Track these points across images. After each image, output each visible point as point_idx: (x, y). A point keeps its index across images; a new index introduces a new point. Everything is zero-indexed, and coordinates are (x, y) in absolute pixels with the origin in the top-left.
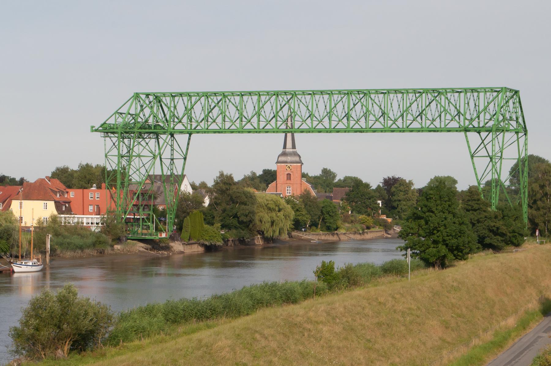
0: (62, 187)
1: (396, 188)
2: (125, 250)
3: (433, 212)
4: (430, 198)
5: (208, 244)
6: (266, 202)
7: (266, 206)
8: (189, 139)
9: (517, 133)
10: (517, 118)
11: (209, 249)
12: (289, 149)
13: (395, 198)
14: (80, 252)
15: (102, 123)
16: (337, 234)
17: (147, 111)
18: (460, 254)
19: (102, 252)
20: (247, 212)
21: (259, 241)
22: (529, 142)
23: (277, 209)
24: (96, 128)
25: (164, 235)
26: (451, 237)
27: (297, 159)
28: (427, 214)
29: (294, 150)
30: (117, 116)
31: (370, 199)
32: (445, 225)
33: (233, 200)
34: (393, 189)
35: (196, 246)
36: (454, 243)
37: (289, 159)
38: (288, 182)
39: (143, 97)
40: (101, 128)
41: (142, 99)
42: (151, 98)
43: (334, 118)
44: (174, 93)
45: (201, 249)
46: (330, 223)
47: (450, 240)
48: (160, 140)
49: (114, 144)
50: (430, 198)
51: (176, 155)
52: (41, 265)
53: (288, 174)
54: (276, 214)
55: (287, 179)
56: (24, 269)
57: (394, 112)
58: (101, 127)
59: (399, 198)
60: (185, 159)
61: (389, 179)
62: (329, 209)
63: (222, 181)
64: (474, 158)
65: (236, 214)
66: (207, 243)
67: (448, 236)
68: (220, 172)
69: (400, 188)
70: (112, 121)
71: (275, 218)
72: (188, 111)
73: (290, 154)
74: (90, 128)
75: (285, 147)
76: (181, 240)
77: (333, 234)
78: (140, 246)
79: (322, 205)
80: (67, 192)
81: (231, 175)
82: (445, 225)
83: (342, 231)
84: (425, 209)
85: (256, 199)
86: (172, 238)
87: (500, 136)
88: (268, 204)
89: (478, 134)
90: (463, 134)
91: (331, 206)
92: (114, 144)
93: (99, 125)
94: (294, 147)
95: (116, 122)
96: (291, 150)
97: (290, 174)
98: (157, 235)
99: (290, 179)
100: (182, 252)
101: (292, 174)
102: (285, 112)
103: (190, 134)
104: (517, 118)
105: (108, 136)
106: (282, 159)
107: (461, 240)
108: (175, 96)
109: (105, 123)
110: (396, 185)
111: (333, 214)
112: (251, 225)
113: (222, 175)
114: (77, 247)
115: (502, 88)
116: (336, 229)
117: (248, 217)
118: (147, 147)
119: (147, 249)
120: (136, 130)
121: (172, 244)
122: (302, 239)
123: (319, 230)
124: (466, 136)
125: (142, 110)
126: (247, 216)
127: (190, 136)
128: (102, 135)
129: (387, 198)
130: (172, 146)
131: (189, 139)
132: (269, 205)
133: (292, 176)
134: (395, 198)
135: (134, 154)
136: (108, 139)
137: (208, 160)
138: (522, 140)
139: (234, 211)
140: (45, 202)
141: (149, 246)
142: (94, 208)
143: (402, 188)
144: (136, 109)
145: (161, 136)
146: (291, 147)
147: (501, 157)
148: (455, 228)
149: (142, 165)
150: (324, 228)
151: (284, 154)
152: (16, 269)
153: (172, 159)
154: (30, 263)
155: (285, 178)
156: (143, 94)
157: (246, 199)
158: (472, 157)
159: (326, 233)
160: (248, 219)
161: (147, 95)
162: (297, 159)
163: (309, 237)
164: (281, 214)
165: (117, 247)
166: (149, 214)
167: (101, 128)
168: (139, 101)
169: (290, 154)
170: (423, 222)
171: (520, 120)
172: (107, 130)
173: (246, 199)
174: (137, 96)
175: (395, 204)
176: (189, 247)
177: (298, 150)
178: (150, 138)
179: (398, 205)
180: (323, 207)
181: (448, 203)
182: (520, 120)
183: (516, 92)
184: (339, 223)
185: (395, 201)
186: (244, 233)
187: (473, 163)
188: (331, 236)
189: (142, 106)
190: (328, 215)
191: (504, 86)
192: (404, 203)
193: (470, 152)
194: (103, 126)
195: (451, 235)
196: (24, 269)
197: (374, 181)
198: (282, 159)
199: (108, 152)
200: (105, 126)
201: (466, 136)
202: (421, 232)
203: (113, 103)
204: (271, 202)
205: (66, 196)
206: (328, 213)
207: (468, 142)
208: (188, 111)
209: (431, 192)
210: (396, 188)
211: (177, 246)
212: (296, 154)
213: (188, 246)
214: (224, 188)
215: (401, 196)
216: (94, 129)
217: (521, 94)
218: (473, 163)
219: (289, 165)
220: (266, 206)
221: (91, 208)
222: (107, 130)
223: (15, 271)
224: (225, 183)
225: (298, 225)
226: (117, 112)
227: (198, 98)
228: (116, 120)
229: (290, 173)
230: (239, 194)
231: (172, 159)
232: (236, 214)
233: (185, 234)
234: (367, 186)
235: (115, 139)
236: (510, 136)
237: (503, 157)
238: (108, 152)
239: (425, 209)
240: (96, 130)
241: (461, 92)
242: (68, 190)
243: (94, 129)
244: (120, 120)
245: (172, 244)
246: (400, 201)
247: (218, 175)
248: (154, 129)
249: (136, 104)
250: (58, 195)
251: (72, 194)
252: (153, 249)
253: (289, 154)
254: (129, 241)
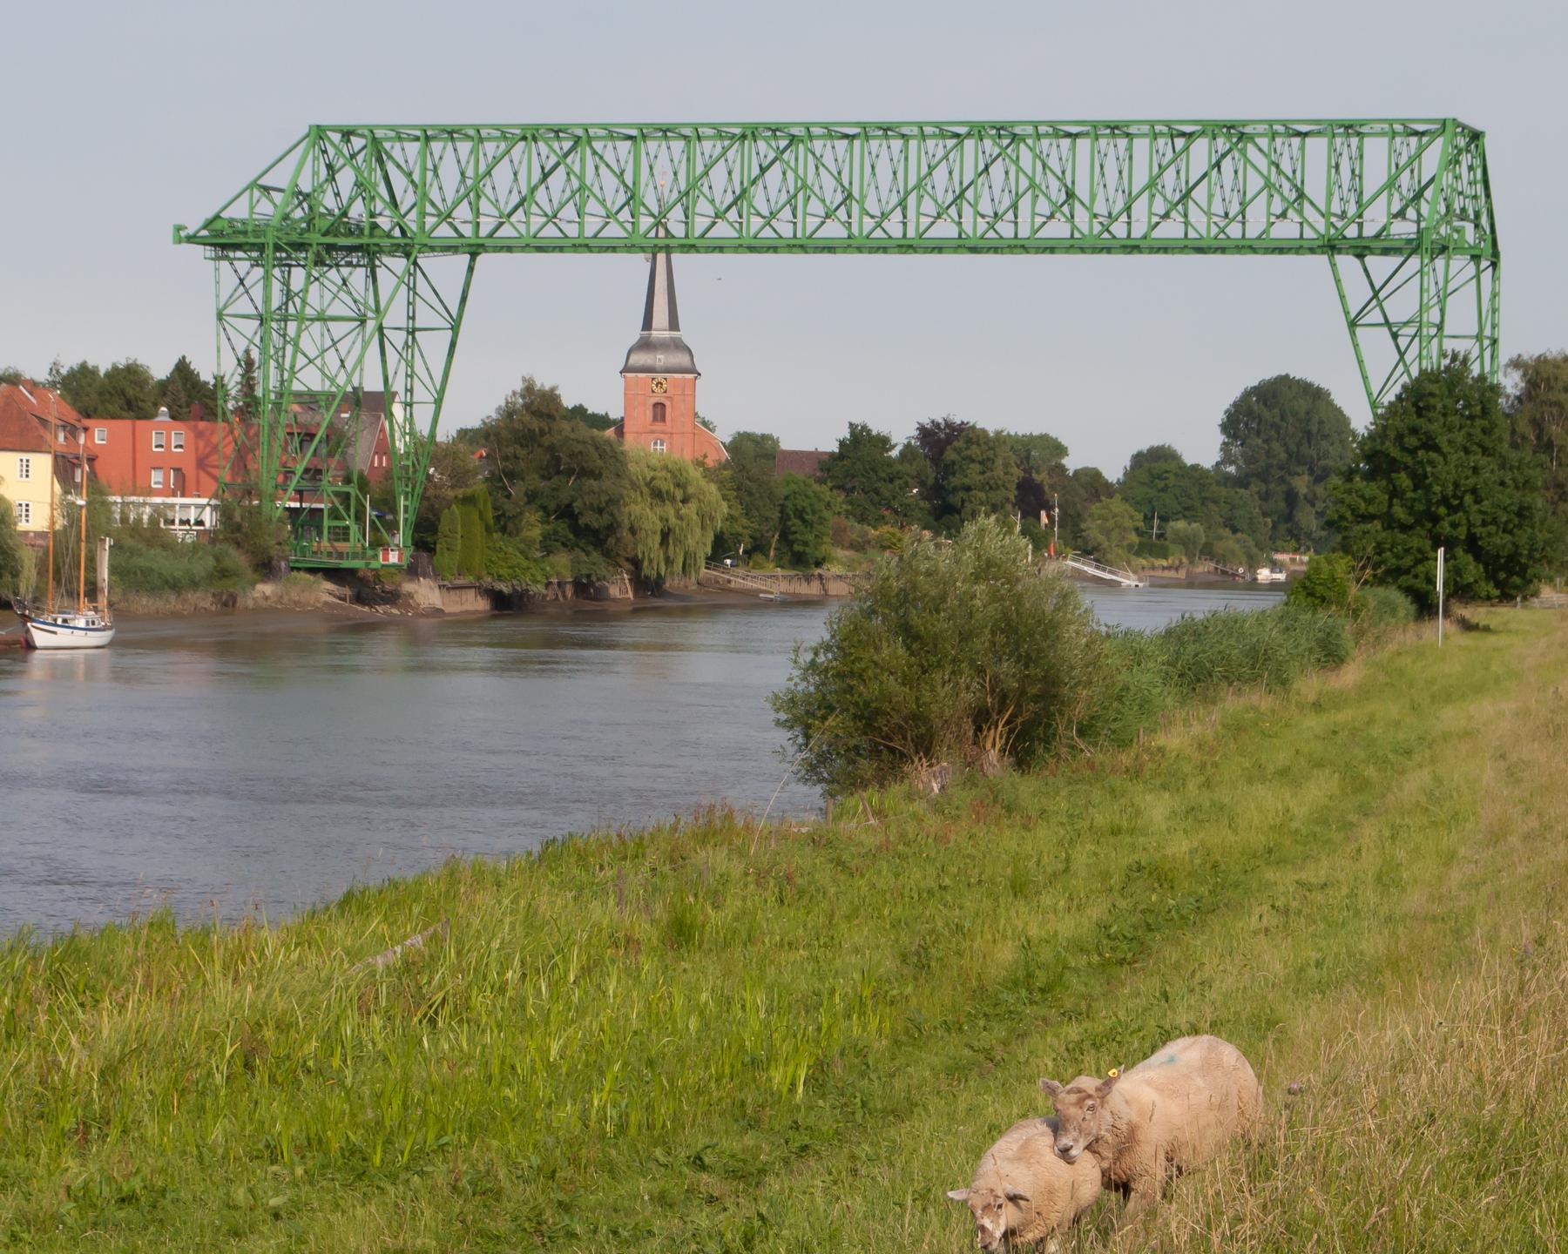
0: (72, 415)
1: (958, 451)
2: (286, 599)
3: (1437, 449)
4: (1428, 408)
5: (505, 590)
6: (649, 474)
7: (648, 484)
8: (471, 269)
9: (1476, 258)
10: (1477, 215)
11: (504, 604)
12: (660, 331)
13: (956, 481)
14: (172, 598)
15: (210, 214)
16: (820, 576)
17: (346, 179)
18: (1516, 580)
19: (228, 603)
20: (604, 498)
21: (620, 589)
22: (1505, 286)
23: (679, 494)
24: (191, 231)
25: (393, 558)
26: (1492, 529)
27: (681, 359)
28: (1421, 453)
29: (675, 334)
30: (256, 193)
31: (891, 481)
32: (1474, 491)
33: (554, 467)
34: (950, 455)
35: (471, 594)
36: (1504, 546)
37: (661, 359)
38: (659, 426)
39: (336, 137)
40: (204, 233)
41: (332, 143)
42: (357, 143)
43: (703, 206)
44: (432, 127)
45: (481, 605)
46: (806, 544)
47: (1489, 535)
48: (380, 272)
49: (242, 281)
50: (1428, 408)
51: (424, 317)
52: (110, 628)
53: (656, 405)
54: (678, 511)
55: (655, 419)
56: (64, 637)
57: (879, 193)
58: (204, 227)
59: (966, 481)
60: (455, 328)
61: (936, 425)
62: (802, 502)
63: (527, 407)
64: (1358, 330)
65: (569, 506)
66: (504, 588)
67: (1484, 524)
68: (524, 380)
69: (969, 453)
70: (239, 211)
71: (673, 520)
72: (472, 193)
73: (664, 346)
74: (170, 235)
75: (648, 324)
76: (437, 575)
77: (808, 579)
78: (325, 591)
79: (785, 491)
80: (86, 429)
81: (553, 390)
82: (1474, 491)
83: (836, 570)
84: (1412, 441)
85: (624, 464)
86: (413, 571)
87: (1440, 263)
88: (653, 479)
89: (1357, 262)
90: (1322, 260)
91: (810, 493)
92: (242, 281)
93: (201, 223)
94: (674, 324)
95: (252, 212)
96: (667, 334)
97: (663, 405)
98: (376, 557)
99: (663, 419)
100: (438, 612)
101: (667, 403)
102: (766, 184)
103: (474, 256)
104: (1477, 215)
105: (227, 258)
106: (640, 359)
107: (1523, 537)
108: (435, 138)
109: (217, 217)
110: (956, 444)
111: (815, 518)
112: (611, 541)
113: (529, 389)
114: (167, 582)
115: (1444, 122)
116: (818, 564)
117: (605, 516)
118: (342, 295)
119: (343, 599)
120: (315, 238)
121: (408, 587)
122: (731, 591)
123: (771, 566)
124: (1333, 265)
125: (332, 178)
126: (600, 511)
127: (473, 259)
128: (208, 254)
129: (931, 481)
130: (412, 289)
131: (471, 269)
132: (657, 483)
133: (668, 410)
134: (956, 481)
135: (309, 311)
136: (224, 264)
137: (517, 337)
138: (1487, 276)
139: (564, 497)
140: (25, 456)
141: (347, 591)
142: (167, 477)
143: (974, 451)
144: (315, 173)
145: (386, 260)
146: (666, 323)
147: (1440, 327)
148: (1508, 501)
149: (328, 343)
150: (787, 558)
151: (645, 345)
152: (40, 638)
153: (412, 332)
154: (81, 623)
155: (649, 414)
156: (334, 129)
157: (600, 463)
158: (1353, 324)
159: (793, 573)
160: (605, 520)
161: (347, 134)
162: (681, 359)
163: (750, 584)
164: (690, 510)
165: (266, 589)
166: (348, 495)
167: (204, 233)
168: (325, 152)
169: (664, 346)
170: (1404, 480)
171: (1484, 220)
172: (223, 239)
173: (600, 463)
174: (319, 133)
175: (955, 500)
176: (454, 595)
177: (685, 334)
178: (349, 264)
179: (963, 501)
180: (786, 498)
181: (1478, 422)
182: (1484, 220)
183: (1476, 136)
184: (826, 548)
185: (955, 490)
186: (593, 562)
187: (1356, 346)
188: (805, 584)
189: (329, 167)
190: (797, 521)
191: (1449, 115)
192: (982, 495)
193: (1347, 313)
194: (212, 227)
195: (1494, 521)
196: (64, 637)
197: (900, 431)
198: (640, 359)
199: (225, 306)
200: (218, 225)
201: (1333, 265)
202: (1400, 512)
203: (245, 155)
204: (664, 473)
205: (82, 440)
206: (800, 514)
207: (1338, 281)
208: (472, 193)
209: (1434, 388)
210: (958, 451)
211: (426, 593)
212: (679, 346)
213: (452, 593)
214: (536, 425)
215: (974, 475)
216: (183, 234)
217: (1488, 142)
218: (1356, 346)
219: (660, 377)
220: (648, 484)
221: (156, 478)
222: (223, 239)
223: (38, 644)
224: (537, 413)
225: (721, 548)
226: (254, 185)
227: (503, 146)
228: (252, 208)
229: (663, 400)
230: (580, 447)
231: (412, 332)
232: (569, 506)
233: (443, 558)
234: (883, 442)
235: (243, 267)
236: (1460, 266)
237: (1448, 329)
238: (225, 306)
239: (1412, 441)
240: (191, 239)
241: (1306, 135)
242: (87, 422)
243: (183, 234)
244: (265, 208)
245: (408, 587)
246: (968, 489)
247: (519, 386)
248: (371, 235)
249: (315, 158)
250: (61, 436)
251: (100, 434)
252: (359, 599)
253: (659, 350)
254: (295, 573)
